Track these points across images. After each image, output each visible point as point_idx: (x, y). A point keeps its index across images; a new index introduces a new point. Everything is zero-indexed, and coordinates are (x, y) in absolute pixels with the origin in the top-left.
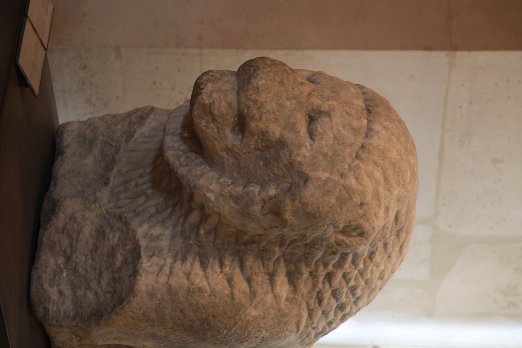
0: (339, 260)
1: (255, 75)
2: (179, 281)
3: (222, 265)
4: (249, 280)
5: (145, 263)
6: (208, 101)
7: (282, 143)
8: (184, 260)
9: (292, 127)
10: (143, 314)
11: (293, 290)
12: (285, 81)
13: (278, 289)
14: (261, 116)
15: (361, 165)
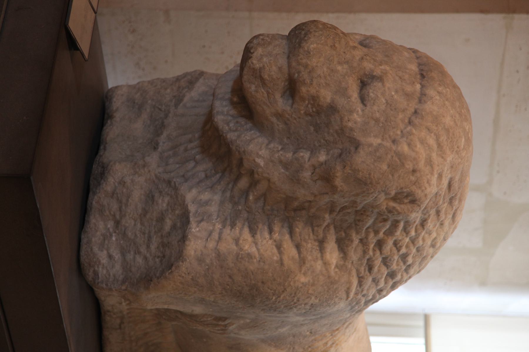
0: (390, 227)
1: (306, 38)
2: (228, 246)
3: (271, 231)
4: (298, 247)
5: (194, 229)
6: (258, 65)
7: (333, 109)
8: (233, 225)
9: (343, 92)
10: (192, 279)
11: (342, 257)
12: (337, 45)
13: (328, 256)
14: (312, 80)
15: (414, 131)
